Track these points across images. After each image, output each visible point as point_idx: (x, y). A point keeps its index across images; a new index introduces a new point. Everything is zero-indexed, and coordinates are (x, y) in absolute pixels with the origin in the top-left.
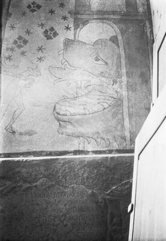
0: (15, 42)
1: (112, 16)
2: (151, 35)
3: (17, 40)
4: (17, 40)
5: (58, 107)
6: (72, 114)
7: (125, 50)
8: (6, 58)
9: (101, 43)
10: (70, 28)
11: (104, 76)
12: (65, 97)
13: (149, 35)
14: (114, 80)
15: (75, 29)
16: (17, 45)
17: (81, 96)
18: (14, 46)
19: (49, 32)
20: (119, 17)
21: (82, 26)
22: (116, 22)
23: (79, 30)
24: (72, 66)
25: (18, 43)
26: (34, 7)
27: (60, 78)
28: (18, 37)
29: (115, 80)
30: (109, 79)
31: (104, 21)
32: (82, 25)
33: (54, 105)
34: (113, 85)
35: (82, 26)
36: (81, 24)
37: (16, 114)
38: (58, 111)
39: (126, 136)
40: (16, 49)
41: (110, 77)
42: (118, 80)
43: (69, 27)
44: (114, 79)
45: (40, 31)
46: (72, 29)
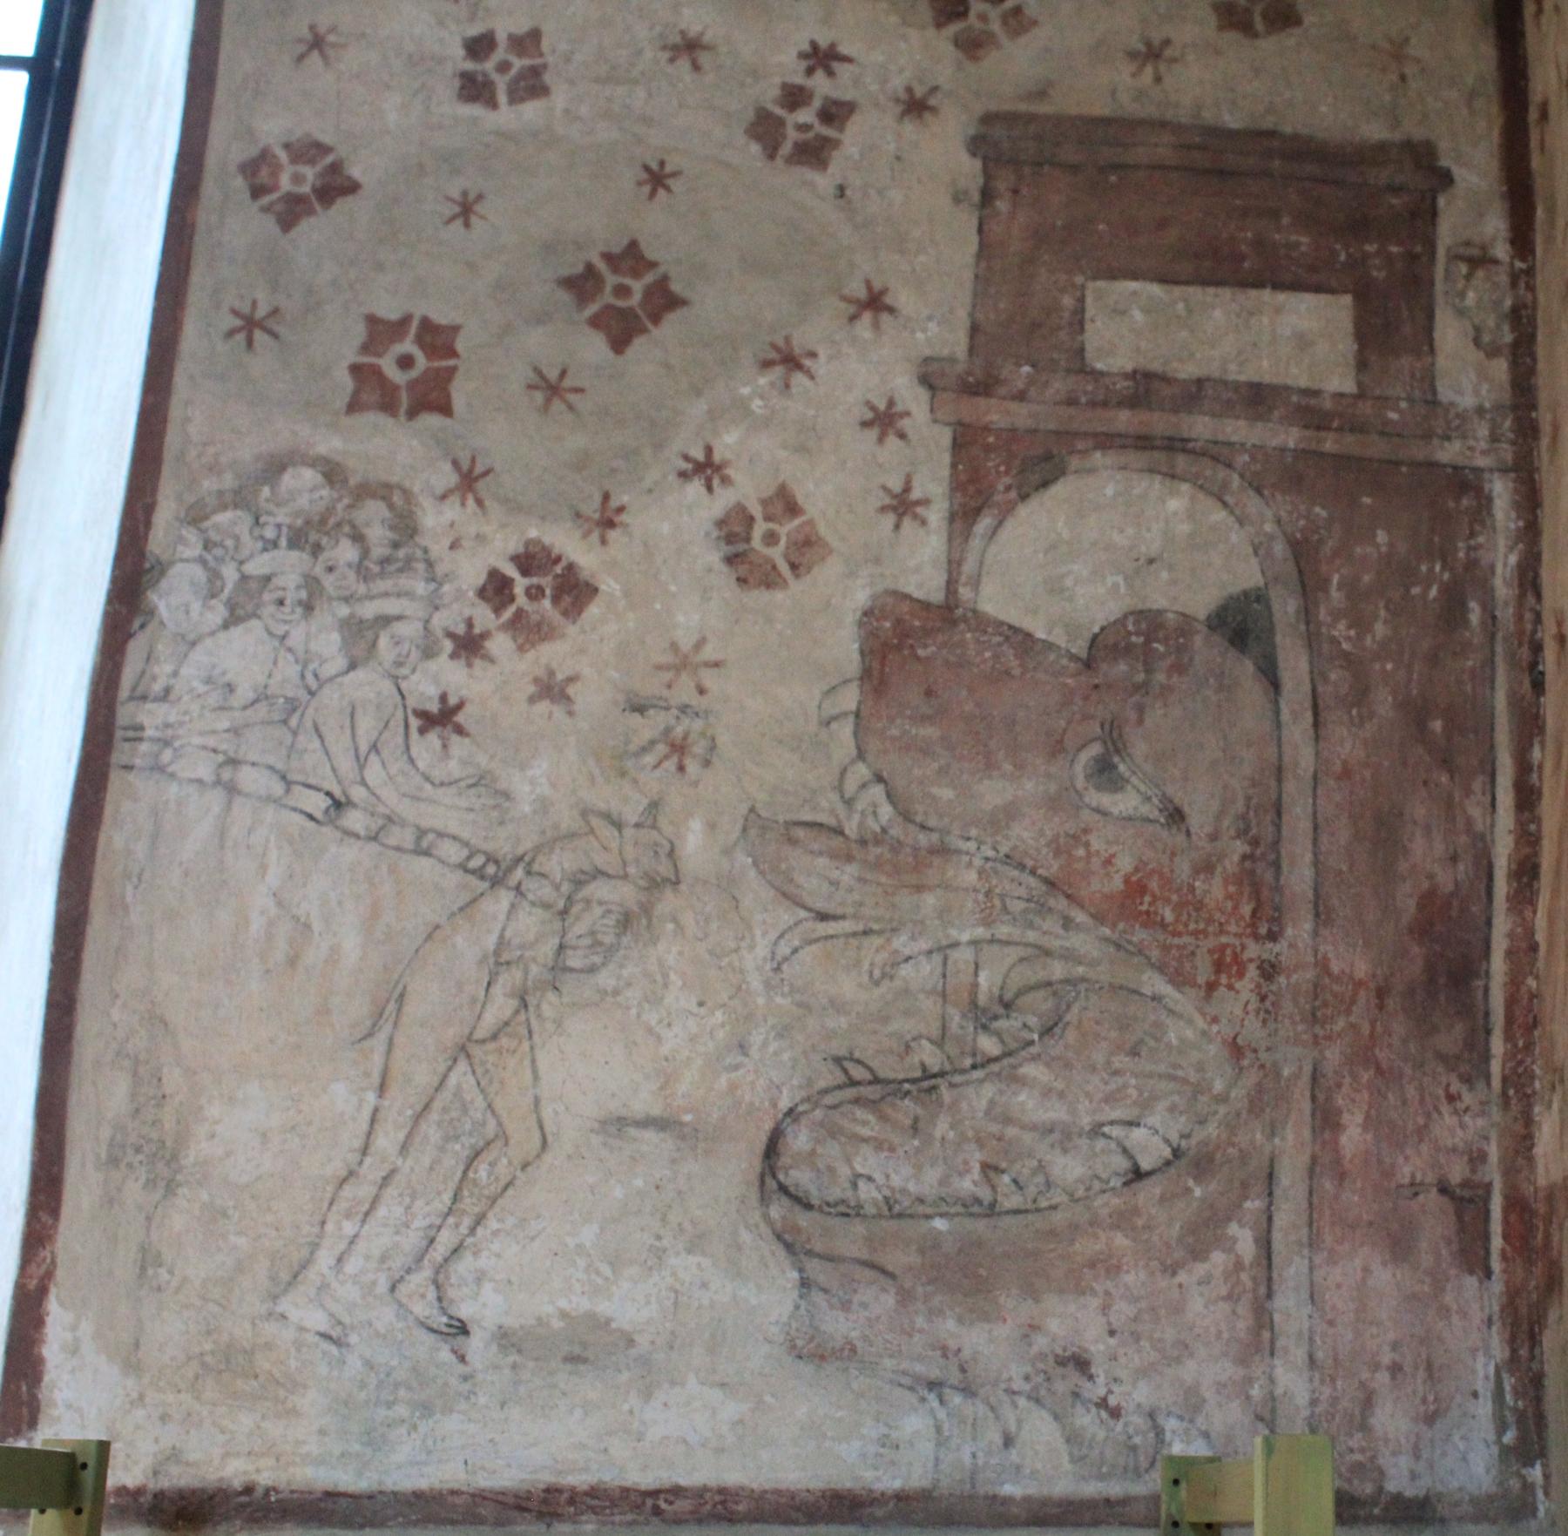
0: (496, 589)
1: (1238, 430)
2: (1521, 597)
3: (511, 571)
4: (511, 571)
5: (799, 1140)
6: (897, 1208)
7: (1316, 714)
8: (423, 715)
9: (1148, 641)
10: (918, 503)
11: (1150, 920)
12: (858, 1073)
13: (1503, 588)
14: (1223, 948)
15: (964, 516)
16: (779, 111)
17: (974, 1067)
18: (484, 616)
19: (760, 528)
20: (1292, 438)
21: (1013, 494)
22: (1287, 475)
23: (984, 523)
24: (919, 819)
25: (521, 600)
26: (535, 593)
27: (823, 917)
28: (1030, 1301)
29: (1228, 952)
30: (1186, 939)
31: (1181, 461)
32: (1008, 488)
33: (768, 1126)
34: (1211, 987)
35: (1013, 494)
36: (1007, 480)
37: (475, 1183)
38: (800, 1177)
39: (1279, 1391)
40: (501, 644)
41: (1192, 926)
42: (1253, 950)
43: (916, 494)
44: (1224, 939)
45: (680, 520)
46: (936, 515)
